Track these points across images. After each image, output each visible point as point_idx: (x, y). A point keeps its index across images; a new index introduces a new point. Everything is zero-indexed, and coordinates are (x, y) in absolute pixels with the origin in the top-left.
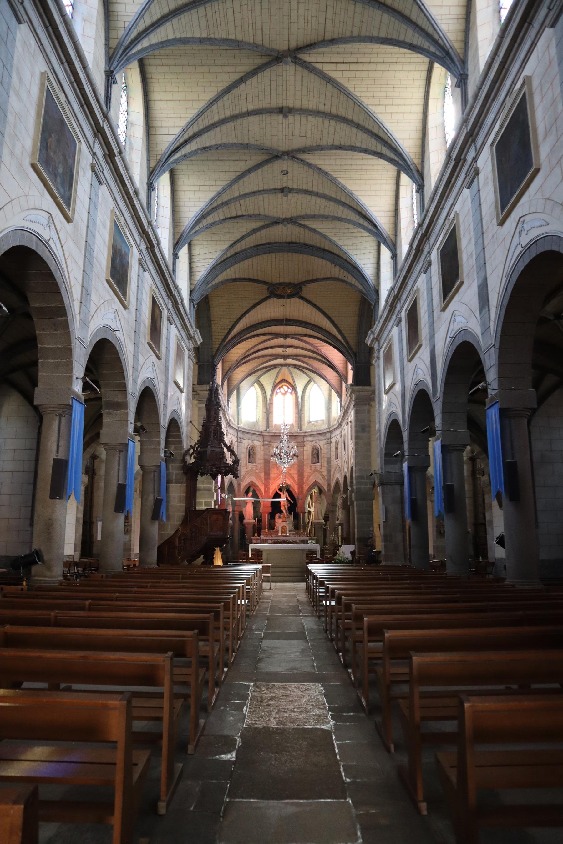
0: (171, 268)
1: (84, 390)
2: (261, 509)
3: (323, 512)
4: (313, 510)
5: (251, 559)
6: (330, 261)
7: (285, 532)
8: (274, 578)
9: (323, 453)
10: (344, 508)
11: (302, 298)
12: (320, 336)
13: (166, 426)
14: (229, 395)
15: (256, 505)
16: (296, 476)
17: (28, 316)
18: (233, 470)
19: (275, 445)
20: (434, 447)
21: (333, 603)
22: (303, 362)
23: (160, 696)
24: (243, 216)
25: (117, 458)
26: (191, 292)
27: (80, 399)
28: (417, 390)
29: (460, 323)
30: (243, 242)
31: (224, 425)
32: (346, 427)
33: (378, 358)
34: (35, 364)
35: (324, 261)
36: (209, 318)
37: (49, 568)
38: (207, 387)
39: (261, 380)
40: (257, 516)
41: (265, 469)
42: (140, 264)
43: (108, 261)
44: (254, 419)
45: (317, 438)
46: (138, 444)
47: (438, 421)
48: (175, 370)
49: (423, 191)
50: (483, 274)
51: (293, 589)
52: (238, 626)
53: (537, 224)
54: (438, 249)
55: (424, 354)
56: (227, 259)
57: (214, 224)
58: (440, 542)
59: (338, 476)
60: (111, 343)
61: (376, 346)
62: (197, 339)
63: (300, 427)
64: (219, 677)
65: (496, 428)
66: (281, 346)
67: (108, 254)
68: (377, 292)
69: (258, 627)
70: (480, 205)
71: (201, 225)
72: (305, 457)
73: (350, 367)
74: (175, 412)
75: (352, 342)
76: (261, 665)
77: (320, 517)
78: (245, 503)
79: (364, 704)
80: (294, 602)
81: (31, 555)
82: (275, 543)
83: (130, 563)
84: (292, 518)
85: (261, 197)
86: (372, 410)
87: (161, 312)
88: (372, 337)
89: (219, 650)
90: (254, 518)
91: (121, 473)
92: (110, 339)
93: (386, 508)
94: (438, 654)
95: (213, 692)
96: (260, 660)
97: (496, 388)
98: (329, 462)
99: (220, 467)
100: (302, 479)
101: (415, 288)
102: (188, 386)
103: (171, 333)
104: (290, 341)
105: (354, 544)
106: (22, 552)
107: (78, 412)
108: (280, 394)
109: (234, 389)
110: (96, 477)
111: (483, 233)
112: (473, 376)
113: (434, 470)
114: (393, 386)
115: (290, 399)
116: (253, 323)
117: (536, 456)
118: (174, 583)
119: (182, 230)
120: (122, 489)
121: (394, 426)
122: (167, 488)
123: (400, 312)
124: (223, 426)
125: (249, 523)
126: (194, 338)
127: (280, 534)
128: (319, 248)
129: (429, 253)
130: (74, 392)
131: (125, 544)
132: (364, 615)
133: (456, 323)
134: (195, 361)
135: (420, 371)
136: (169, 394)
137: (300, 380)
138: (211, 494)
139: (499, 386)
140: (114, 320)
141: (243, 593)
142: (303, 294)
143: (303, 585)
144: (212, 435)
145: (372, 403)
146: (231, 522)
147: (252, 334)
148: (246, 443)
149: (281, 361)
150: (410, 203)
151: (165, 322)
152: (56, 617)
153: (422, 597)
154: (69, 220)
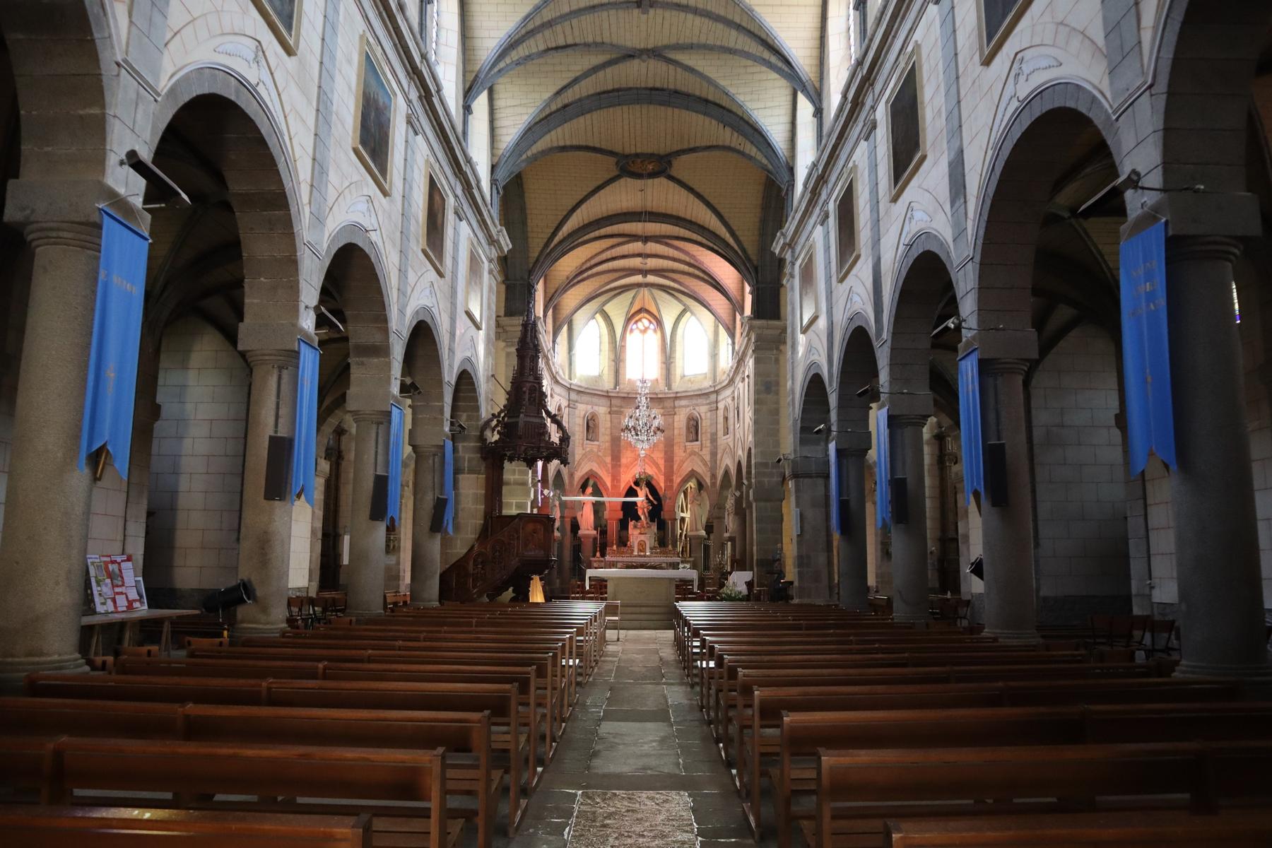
0: (459, 129)
1: (319, 325)
2: (606, 514)
3: (704, 520)
4: (688, 516)
5: (589, 592)
6: (716, 119)
7: (644, 550)
8: (626, 624)
9: (705, 425)
10: (736, 513)
11: (671, 178)
12: (699, 238)
13: (453, 382)
14: (556, 332)
15: (598, 507)
16: (661, 463)
17: (227, 207)
18: (560, 452)
19: (629, 411)
20: (878, 417)
21: (712, 664)
22: (674, 280)
23: (425, 814)
24: (575, 45)
25: (374, 435)
26: (493, 168)
27: (313, 341)
28: (853, 327)
29: (920, 221)
30: (576, 87)
31: (546, 384)
32: (741, 385)
33: (792, 276)
34: (239, 284)
35: (707, 120)
36: (523, 210)
37: (265, 610)
38: (518, 321)
39: (605, 308)
40: (600, 526)
41: (613, 451)
42: (409, 122)
43: (355, 117)
44: (595, 372)
45: (694, 402)
46: (409, 412)
47: (884, 377)
48: (467, 293)
49: (865, 8)
50: (958, 144)
51: (654, 641)
52: (562, 700)
53: (1045, 63)
54: (887, 102)
55: (863, 271)
56: (551, 114)
57: (529, 58)
58: (882, 566)
59: (727, 462)
60: (362, 250)
61: (788, 257)
62: (503, 243)
63: (669, 385)
64: (529, 782)
65: (973, 391)
66: (639, 255)
67: (356, 106)
68: (791, 170)
69: (596, 702)
70: (954, 31)
71: (508, 60)
72: (676, 432)
73: (748, 288)
74: (468, 360)
75: (752, 250)
76: (596, 762)
77: (700, 527)
78: (582, 504)
79: (753, 825)
80: (653, 661)
81: (235, 589)
82: (628, 567)
83: (398, 599)
84: (654, 528)
85: (605, 14)
86: (781, 358)
87: (443, 200)
88: (782, 241)
89: (528, 740)
90: (596, 529)
91: (380, 458)
92: (360, 245)
93: (801, 515)
94: (863, 752)
95: (517, 806)
96: (595, 754)
97: (974, 326)
98: (714, 440)
99: (539, 448)
100: (672, 467)
101: (851, 165)
102: (489, 319)
103: (461, 235)
104: (653, 247)
105: (751, 569)
106: (223, 583)
107: (309, 362)
108: (636, 333)
109: (563, 322)
110: (344, 463)
111: (957, 78)
112: (941, 305)
113: (878, 452)
114: (814, 319)
115: (653, 339)
116: (592, 218)
117: (1038, 433)
118: (462, 632)
119: (477, 68)
120: (381, 484)
121: (815, 384)
122: (456, 482)
123: (826, 202)
124: (545, 382)
125: (587, 536)
126: (498, 242)
127: (636, 553)
128: (700, 98)
129: (873, 108)
130: (302, 330)
131: (388, 569)
132: (755, 687)
133: (913, 222)
134: (500, 279)
135: (856, 298)
136: (458, 333)
137: (669, 309)
138: (524, 491)
139: (980, 322)
140: (367, 214)
141: (571, 648)
142: (674, 173)
143: (670, 634)
144: (527, 397)
145: (782, 347)
146: (557, 534)
147: (592, 235)
148: (583, 409)
149: (638, 278)
150: (844, 27)
151: (450, 216)
152: (269, 689)
153: (850, 657)
154: (289, 51)
